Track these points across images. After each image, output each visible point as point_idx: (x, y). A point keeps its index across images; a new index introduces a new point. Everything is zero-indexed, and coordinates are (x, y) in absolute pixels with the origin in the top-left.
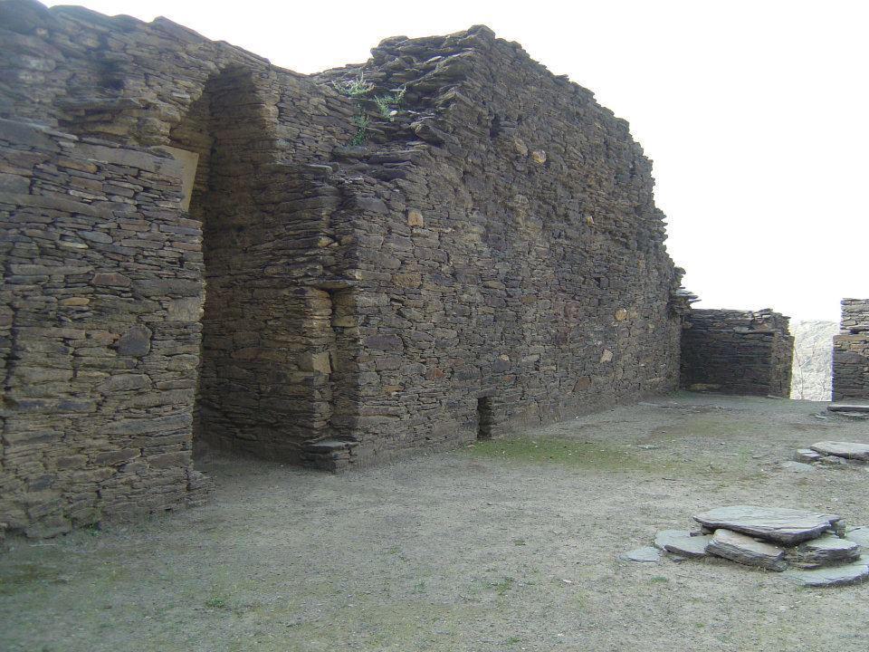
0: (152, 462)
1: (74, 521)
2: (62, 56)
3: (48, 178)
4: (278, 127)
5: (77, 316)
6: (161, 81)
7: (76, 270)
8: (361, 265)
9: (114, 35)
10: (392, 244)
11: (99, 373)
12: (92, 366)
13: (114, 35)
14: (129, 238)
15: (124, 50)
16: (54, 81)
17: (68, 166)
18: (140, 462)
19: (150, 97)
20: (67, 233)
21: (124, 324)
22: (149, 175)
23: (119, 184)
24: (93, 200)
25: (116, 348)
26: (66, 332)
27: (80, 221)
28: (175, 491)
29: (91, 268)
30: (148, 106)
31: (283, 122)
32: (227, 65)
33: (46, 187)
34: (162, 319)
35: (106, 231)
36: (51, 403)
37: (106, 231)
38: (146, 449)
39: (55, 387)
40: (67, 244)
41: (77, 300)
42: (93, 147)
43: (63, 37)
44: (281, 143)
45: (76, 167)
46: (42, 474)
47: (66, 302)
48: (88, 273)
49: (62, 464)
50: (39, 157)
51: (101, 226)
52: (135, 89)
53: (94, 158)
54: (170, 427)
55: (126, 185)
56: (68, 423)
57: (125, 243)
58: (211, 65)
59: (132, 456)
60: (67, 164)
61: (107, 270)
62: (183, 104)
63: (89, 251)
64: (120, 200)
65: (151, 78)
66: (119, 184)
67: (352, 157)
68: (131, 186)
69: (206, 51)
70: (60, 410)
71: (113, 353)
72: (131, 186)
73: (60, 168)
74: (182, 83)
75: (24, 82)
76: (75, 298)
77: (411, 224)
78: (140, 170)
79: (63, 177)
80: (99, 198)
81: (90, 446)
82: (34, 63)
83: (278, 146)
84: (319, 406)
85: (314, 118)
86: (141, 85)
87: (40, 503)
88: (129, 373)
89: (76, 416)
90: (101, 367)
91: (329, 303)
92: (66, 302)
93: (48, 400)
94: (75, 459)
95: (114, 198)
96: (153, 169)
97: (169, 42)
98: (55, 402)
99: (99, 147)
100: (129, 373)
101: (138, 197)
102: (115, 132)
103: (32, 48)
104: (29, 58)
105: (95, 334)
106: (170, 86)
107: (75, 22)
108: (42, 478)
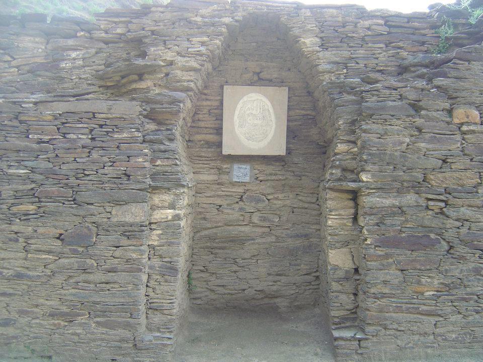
0: (97, 323)
1: (33, 351)
2: (103, 44)
3: (10, 130)
4: (321, 55)
5: (23, 218)
6: (176, 43)
7: (21, 187)
8: (369, 167)
9: (134, 21)
10: (423, 145)
11: (47, 256)
12: (41, 251)
13: (134, 21)
14: (68, 163)
15: (143, 29)
16: (94, 62)
17: (27, 119)
18: (87, 321)
19: (169, 56)
20: (12, 164)
21: (68, 222)
22: (104, 116)
23: (73, 125)
24: (50, 139)
25: (62, 240)
26: (14, 228)
27: (22, 155)
28: (120, 348)
29: (33, 185)
30: (171, 63)
31: (327, 49)
32: (243, 16)
33: (9, 135)
34: (105, 220)
35: (47, 160)
36: (8, 273)
37: (47, 160)
38: (92, 313)
39: (9, 263)
40: (11, 171)
41: (23, 208)
42: (51, 104)
43: (99, 32)
44: (323, 67)
45: (34, 119)
46: (6, 317)
47: (15, 209)
48: (32, 189)
49: (22, 313)
50: (4, 117)
51: (41, 157)
52: (159, 53)
53: (52, 110)
54: (117, 300)
55: (81, 125)
56: (25, 287)
57: (64, 167)
58: (227, 20)
59: (79, 316)
60: (26, 118)
61: (49, 187)
62: (201, 55)
63: (31, 174)
64: (75, 137)
65: (167, 43)
66: (73, 125)
67: (414, 66)
68: (85, 126)
69: (219, 10)
70: (15, 278)
71: (59, 243)
72: (85, 126)
73: (21, 122)
74: (195, 39)
75: (64, 68)
76: (22, 206)
77: (456, 121)
78: (94, 113)
79: (23, 128)
80: (54, 137)
81: (43, 305)
82: (74, 55)
83: (321, 70)
84: (337, 297)
85: (367, 39)
86: (161, 50)
87: (5, 335)
88: (76, 257)
89: (29, 283)
90: (49, 252)
91: (351, 204)
92: (15, 209)
93: (5, 271)
94: (32, 311)
95: (68, 136)
96: (105, 110)
97: (179, 13)
98: (11, 272)
99: (55, 103)
100: (76, 257)
101: (93, 133)
102: (141, 87)
103: (72, 46)
104: (70, 53)
105: (41, 230)
106: (186, 44)
107: (105, 20)
108: (6, 319)
